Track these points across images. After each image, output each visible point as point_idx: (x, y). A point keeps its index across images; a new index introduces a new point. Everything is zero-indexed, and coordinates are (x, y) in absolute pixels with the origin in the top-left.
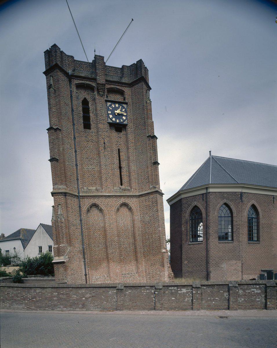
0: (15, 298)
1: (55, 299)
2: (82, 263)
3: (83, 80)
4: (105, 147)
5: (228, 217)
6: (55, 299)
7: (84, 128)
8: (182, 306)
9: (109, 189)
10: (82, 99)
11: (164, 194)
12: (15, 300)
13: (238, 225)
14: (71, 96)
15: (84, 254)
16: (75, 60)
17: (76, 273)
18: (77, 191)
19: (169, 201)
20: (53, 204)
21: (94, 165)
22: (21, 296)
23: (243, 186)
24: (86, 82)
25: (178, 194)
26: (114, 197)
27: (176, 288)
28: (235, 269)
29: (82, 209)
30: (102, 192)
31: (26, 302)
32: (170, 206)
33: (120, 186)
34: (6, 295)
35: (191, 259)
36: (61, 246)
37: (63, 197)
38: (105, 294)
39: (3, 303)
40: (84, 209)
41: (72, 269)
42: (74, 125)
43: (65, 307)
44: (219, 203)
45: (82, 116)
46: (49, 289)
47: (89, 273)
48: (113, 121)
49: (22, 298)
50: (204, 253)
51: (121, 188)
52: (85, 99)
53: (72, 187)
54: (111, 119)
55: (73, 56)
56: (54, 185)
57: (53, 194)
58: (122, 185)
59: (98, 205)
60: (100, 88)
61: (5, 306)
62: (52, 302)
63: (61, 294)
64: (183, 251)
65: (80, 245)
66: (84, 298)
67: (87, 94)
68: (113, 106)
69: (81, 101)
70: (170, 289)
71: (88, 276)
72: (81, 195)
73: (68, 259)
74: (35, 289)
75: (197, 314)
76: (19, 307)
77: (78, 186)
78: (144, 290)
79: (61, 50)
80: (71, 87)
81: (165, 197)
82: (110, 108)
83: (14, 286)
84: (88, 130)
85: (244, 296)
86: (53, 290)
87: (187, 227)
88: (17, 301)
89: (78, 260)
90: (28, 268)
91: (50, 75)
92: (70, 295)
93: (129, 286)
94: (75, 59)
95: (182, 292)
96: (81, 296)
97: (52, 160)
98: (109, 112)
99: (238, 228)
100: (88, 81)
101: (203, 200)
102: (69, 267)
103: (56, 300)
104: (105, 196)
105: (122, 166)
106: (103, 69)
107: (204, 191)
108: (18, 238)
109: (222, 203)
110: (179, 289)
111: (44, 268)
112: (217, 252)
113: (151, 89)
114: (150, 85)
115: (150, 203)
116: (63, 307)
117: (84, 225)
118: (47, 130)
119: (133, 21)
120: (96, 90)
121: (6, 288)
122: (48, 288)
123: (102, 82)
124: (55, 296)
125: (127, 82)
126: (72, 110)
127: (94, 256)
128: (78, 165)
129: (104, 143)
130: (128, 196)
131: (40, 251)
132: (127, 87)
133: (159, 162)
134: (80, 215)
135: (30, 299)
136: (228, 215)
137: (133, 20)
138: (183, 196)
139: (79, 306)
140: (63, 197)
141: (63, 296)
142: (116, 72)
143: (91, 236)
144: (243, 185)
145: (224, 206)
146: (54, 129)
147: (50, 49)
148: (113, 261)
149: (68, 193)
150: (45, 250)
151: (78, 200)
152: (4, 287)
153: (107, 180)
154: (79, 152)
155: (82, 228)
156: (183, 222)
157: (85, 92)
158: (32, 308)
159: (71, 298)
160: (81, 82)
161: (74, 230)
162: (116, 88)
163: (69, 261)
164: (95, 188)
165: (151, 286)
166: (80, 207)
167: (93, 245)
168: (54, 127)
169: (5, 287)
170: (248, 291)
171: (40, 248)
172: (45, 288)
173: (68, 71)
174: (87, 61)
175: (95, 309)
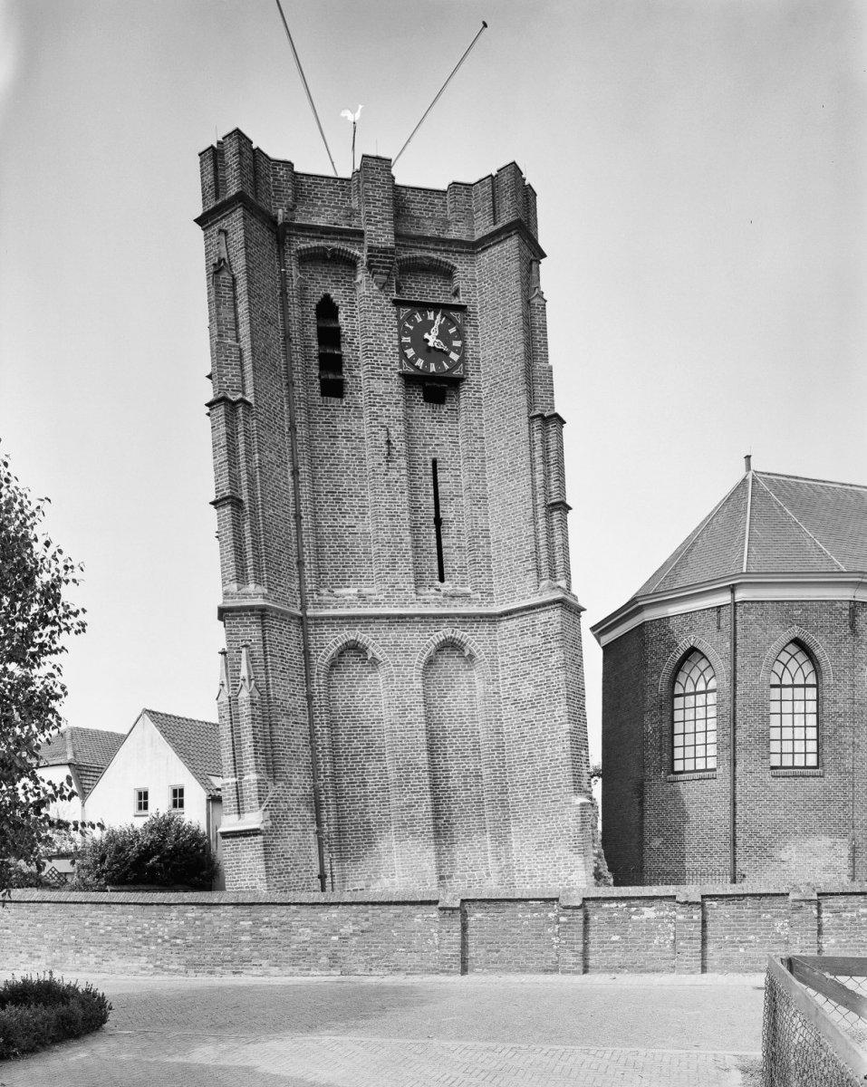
0: (116, 937)
1: (243, 938)
2: (312, 837)
3: (322, 238)
4: (389, 454)
5: (805, 686)
6: (243, 938)
7: (322, 395)
8: (643, 960)
9: (403, 596)
10: (317, 300)
11: (584, 610)
12: (117, 943)
13: (840, 716)
14: (284, 293)
15: (317, 807)
16: (297, 174)
17: (292, 869)
18: (299, 602)
19: (600, 629)
20: (223, 645)
21: (354, 513)
22: (137, 932)
23: (860, 580)
24: (330, 243)
25: (633, 608)
26: (416, 619)
27: (624, 905)
28: (829, 867)
29: (313, 659)
30: (377, 604)
31: (153, 948)
32: (603, 648)
33: (438, 583)
34: (85, 928)
35: (676, 831)
36: (248, 781)
37: (255, 623)
38: (400, 925)
39: (78, 955)
40: (321, 660)
41: (283, 855)
42: (290, 384)
43: (276, 966)
45: (316, 354)
46: (226, 907)
47: (331, 869)
48: (418, 367)
49: (140, 936)
50: (723, 812)
51: (439, 590)
52: (327, 298)
53: (279, 589)
54: (411, 362)
55: (289, 163)
56: (227, 582)
57: (223, 613)
58: (442, 579)
59: (364, 646)
60: (378, 262)
61: (84, 964)
62: (234, 950)
63: (264, 923)
64: (646, 805)
65: (304, 777)
66: (336, 935)
67: (332, 281)
68: (419, 320)
69: (314, 306)
70: (606, 909)
71: (328, 880)
72: (312, 613)
73: (270, 823)
74: (181, 907)
75: (689, 983)
76: (130, 964)
77: (300, 584)
78: (523, 911)
79: (254, 146)
80: (283, 264)
81: (588, 620)
82: (407, 325)
83: (114, 901)
84: (335, 401)
85: (835, 929)
86: (238, 911)
87: (661, 721)
88: (122, 947)
89: (299, 826)
90: (108, 859)
91: (216, 227)
92: (291, 927)
93: (479, 900)
94: (296, 169)
95: (644, 917)
96: (327, 931)
97: (228, 501)
98: (404, 338)
100: (336, 239)
101: (719, 628)
102: (273, 849)
103: (248, 943)
104: (388, 617)
105: (441, 515)
106: (387, 198)
107: (725, 598)
108: (62, 761)
109: (785, 637)
110: (633, 909)
111: (159, 861)
112: (765, 806)
113: (544, 256)
114: (541, 242)
115: (538, 640)
116: (270, 965)
117: (320, 713)
118: (207, 405)
119: (486, 29)
120: (361, 267)
121: (87, 906)
122: (222, 907)
123: (384, 243)
124: (243, 932)
125: (464, 238)
126: (287, 338)
127: (348, 814)
128: (303, 515)
129: (388, 442)
131: (140, 804)
132: (466, 252)
133: (568, 502)
134: (308, 680)
135: (166, 941)
136: (805, 679)
137: (485, 25)
138: (649, 615)
139: (321, 961)
140: (255, 623)
141: (268, 929)
142: (430, 204)
143: (341, 749)
145: (793, 649)
146: (230, 401)
147: (219, 143)
148: (413, 833)
150: (160, 804)
151: (300, 629)
152: (81, 903)
153: (396, 563)
154: (305, 472)
155: (311, 722)
156: (648, 704)
157: (326, 277)
158: (170, 967)
159: (293, 937)
160: (315, 243)
161: (288, 729)
162: (428, 257)
163: (272, 827)
164: (354, 591)
165: (546, 900)
166: (306, 653)
167: (345, 780)
168: (231, 398)
169: (86, 903)
170: (849, 915)
171: (143, 796)
172: (215, 904)
173: (273, 210)
174: (332, 174)
175: (371, 970)
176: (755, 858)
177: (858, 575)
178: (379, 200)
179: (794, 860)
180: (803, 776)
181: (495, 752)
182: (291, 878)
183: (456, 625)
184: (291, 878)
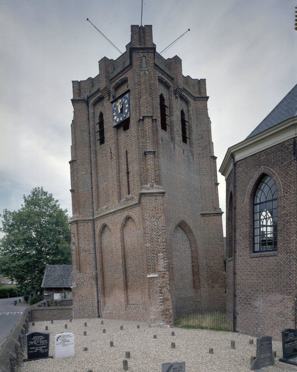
23: (293, 123)
26: (118, 212)
28: (281, 313)
44: (251, 178)
73: (76, 286)
99: (287, 222)
130: (131, 206)
144: (292, 121)
149: (80, 220)
171: (7, 279)
176: (243, 304)
177: (291, 120)
178: (152, 66)
179: (261, 307)
180: (266, 256)
181: (141, 257)
182: (84, 302)
183: (129, 210)
184: (84, 302)
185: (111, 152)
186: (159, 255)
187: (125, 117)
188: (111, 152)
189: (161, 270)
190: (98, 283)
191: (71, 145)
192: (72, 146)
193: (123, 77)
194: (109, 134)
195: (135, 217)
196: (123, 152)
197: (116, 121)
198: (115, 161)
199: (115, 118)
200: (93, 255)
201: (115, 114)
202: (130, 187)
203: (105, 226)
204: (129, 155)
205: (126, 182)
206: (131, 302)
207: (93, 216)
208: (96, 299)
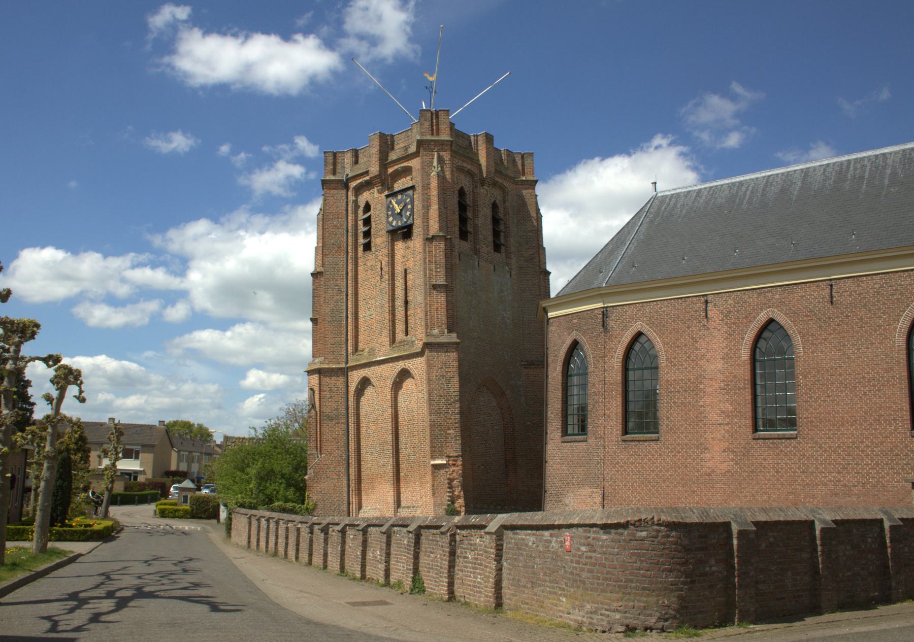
185: (381, 269)
186: (448, 432)
187: (406, 222)
188: (381, 269)
189: (451, 454)
190: (350, 472)
191: (316, 245)
192: (316, 248)
193: (405, 164)
194: (380, 240)
195: (414, 372)
196: (399, 269)
197: (391, 224)
198: (387, 282)
199: (391, 219)
200: (343, 426)
201: (390, 213)
202: (409, 325)
203: (365, 382)
204: (410, 276)
205: (404, 315)
206: (403, 504)
207: (347, 363)
208: (346, 499)
